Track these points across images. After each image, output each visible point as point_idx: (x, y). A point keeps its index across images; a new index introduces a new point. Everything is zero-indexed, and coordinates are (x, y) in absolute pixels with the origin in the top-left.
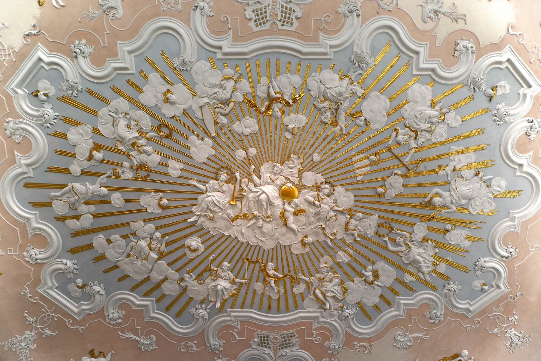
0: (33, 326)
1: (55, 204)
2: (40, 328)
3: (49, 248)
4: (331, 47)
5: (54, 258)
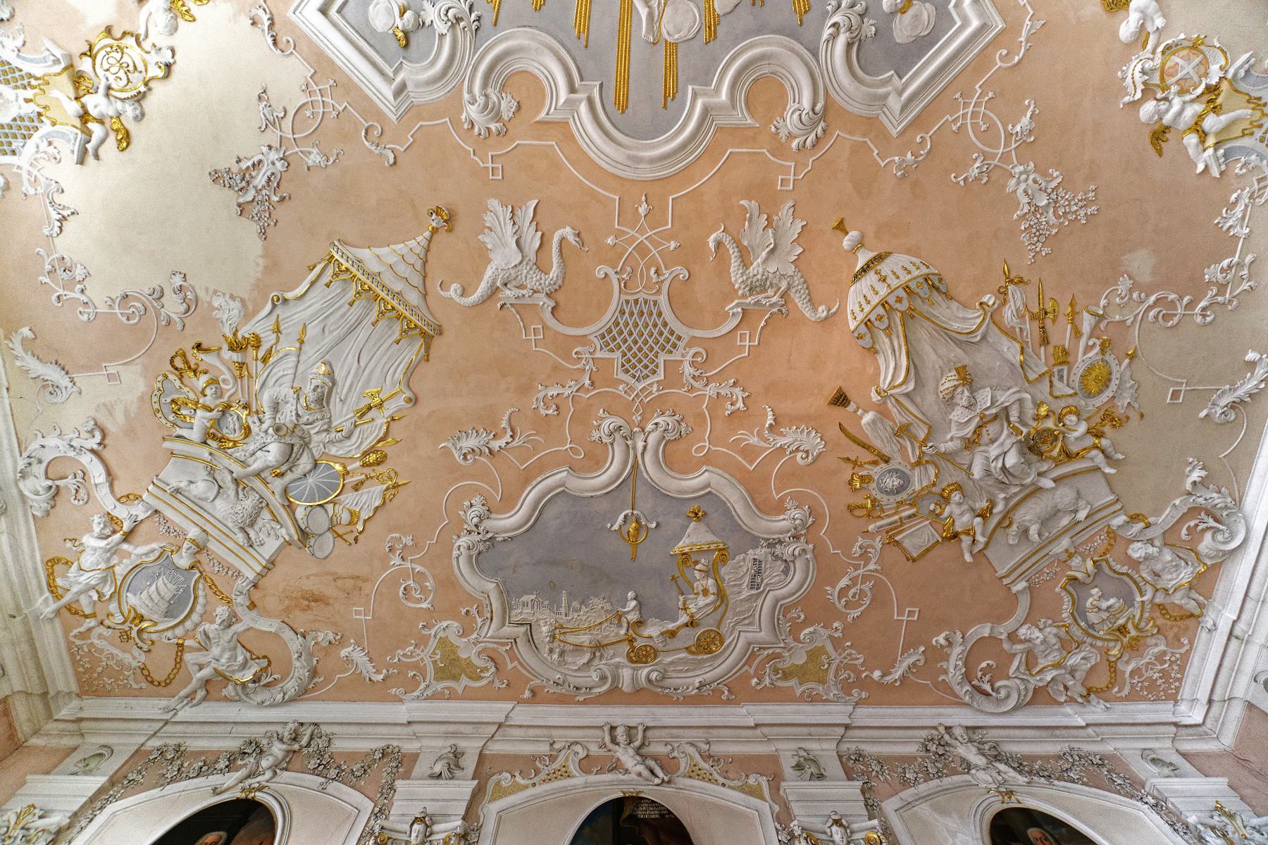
0: (996, 166)
4: (572, 89)
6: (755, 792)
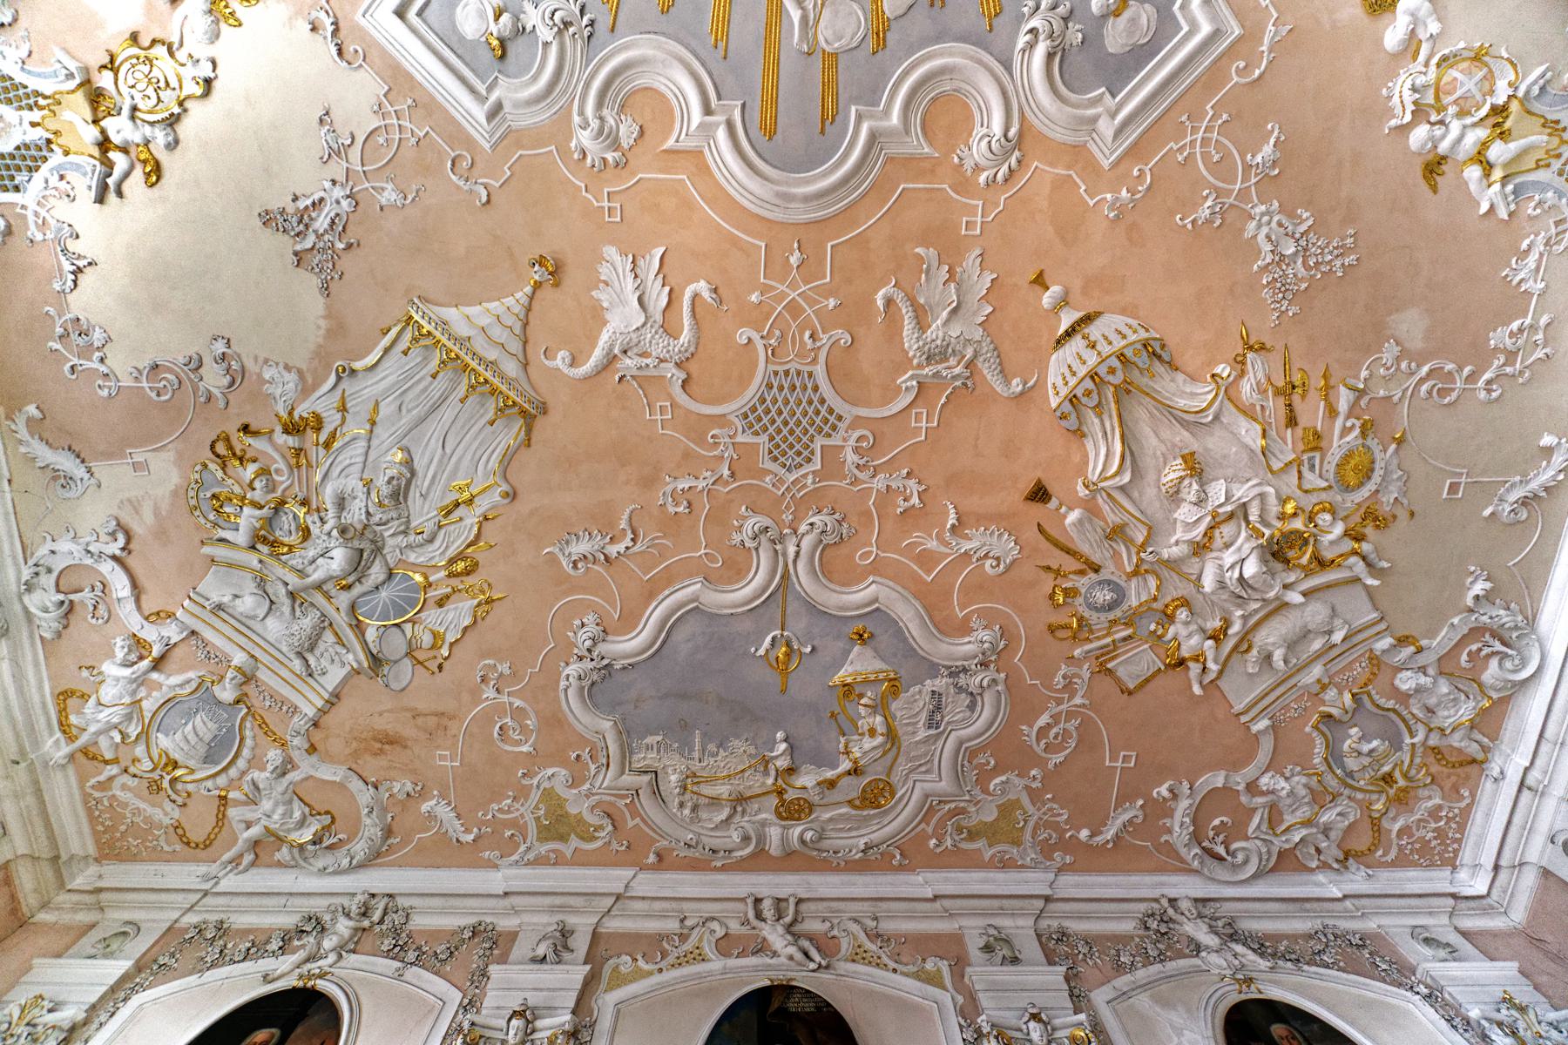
0: (1231, 205)
1: (830, 39)
2: (1242, 183)
3: (975, 94)
4: (708, 111)
5: (1005, 79)
6: (934, 980)
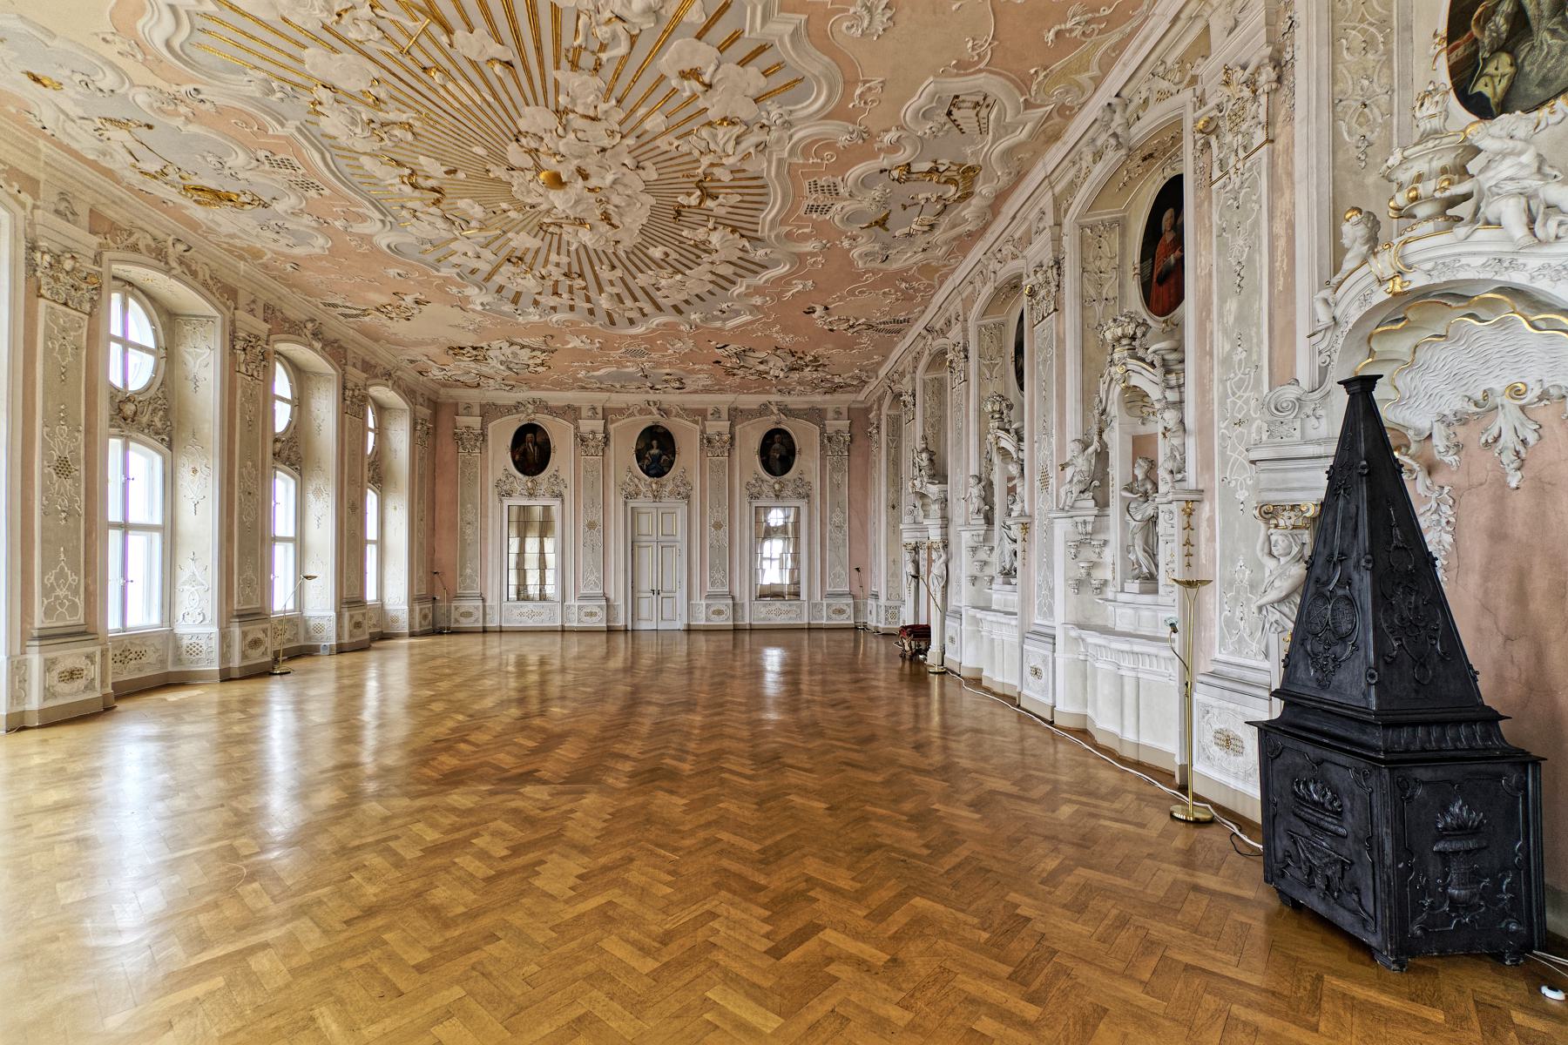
6: (696, 422)
